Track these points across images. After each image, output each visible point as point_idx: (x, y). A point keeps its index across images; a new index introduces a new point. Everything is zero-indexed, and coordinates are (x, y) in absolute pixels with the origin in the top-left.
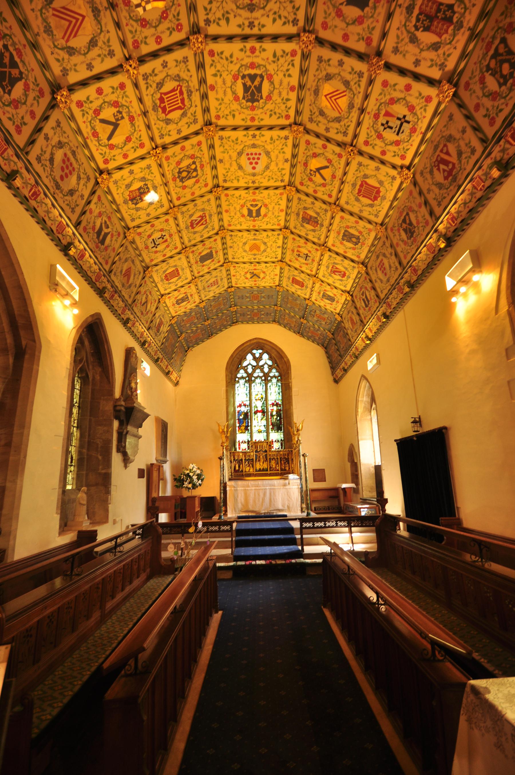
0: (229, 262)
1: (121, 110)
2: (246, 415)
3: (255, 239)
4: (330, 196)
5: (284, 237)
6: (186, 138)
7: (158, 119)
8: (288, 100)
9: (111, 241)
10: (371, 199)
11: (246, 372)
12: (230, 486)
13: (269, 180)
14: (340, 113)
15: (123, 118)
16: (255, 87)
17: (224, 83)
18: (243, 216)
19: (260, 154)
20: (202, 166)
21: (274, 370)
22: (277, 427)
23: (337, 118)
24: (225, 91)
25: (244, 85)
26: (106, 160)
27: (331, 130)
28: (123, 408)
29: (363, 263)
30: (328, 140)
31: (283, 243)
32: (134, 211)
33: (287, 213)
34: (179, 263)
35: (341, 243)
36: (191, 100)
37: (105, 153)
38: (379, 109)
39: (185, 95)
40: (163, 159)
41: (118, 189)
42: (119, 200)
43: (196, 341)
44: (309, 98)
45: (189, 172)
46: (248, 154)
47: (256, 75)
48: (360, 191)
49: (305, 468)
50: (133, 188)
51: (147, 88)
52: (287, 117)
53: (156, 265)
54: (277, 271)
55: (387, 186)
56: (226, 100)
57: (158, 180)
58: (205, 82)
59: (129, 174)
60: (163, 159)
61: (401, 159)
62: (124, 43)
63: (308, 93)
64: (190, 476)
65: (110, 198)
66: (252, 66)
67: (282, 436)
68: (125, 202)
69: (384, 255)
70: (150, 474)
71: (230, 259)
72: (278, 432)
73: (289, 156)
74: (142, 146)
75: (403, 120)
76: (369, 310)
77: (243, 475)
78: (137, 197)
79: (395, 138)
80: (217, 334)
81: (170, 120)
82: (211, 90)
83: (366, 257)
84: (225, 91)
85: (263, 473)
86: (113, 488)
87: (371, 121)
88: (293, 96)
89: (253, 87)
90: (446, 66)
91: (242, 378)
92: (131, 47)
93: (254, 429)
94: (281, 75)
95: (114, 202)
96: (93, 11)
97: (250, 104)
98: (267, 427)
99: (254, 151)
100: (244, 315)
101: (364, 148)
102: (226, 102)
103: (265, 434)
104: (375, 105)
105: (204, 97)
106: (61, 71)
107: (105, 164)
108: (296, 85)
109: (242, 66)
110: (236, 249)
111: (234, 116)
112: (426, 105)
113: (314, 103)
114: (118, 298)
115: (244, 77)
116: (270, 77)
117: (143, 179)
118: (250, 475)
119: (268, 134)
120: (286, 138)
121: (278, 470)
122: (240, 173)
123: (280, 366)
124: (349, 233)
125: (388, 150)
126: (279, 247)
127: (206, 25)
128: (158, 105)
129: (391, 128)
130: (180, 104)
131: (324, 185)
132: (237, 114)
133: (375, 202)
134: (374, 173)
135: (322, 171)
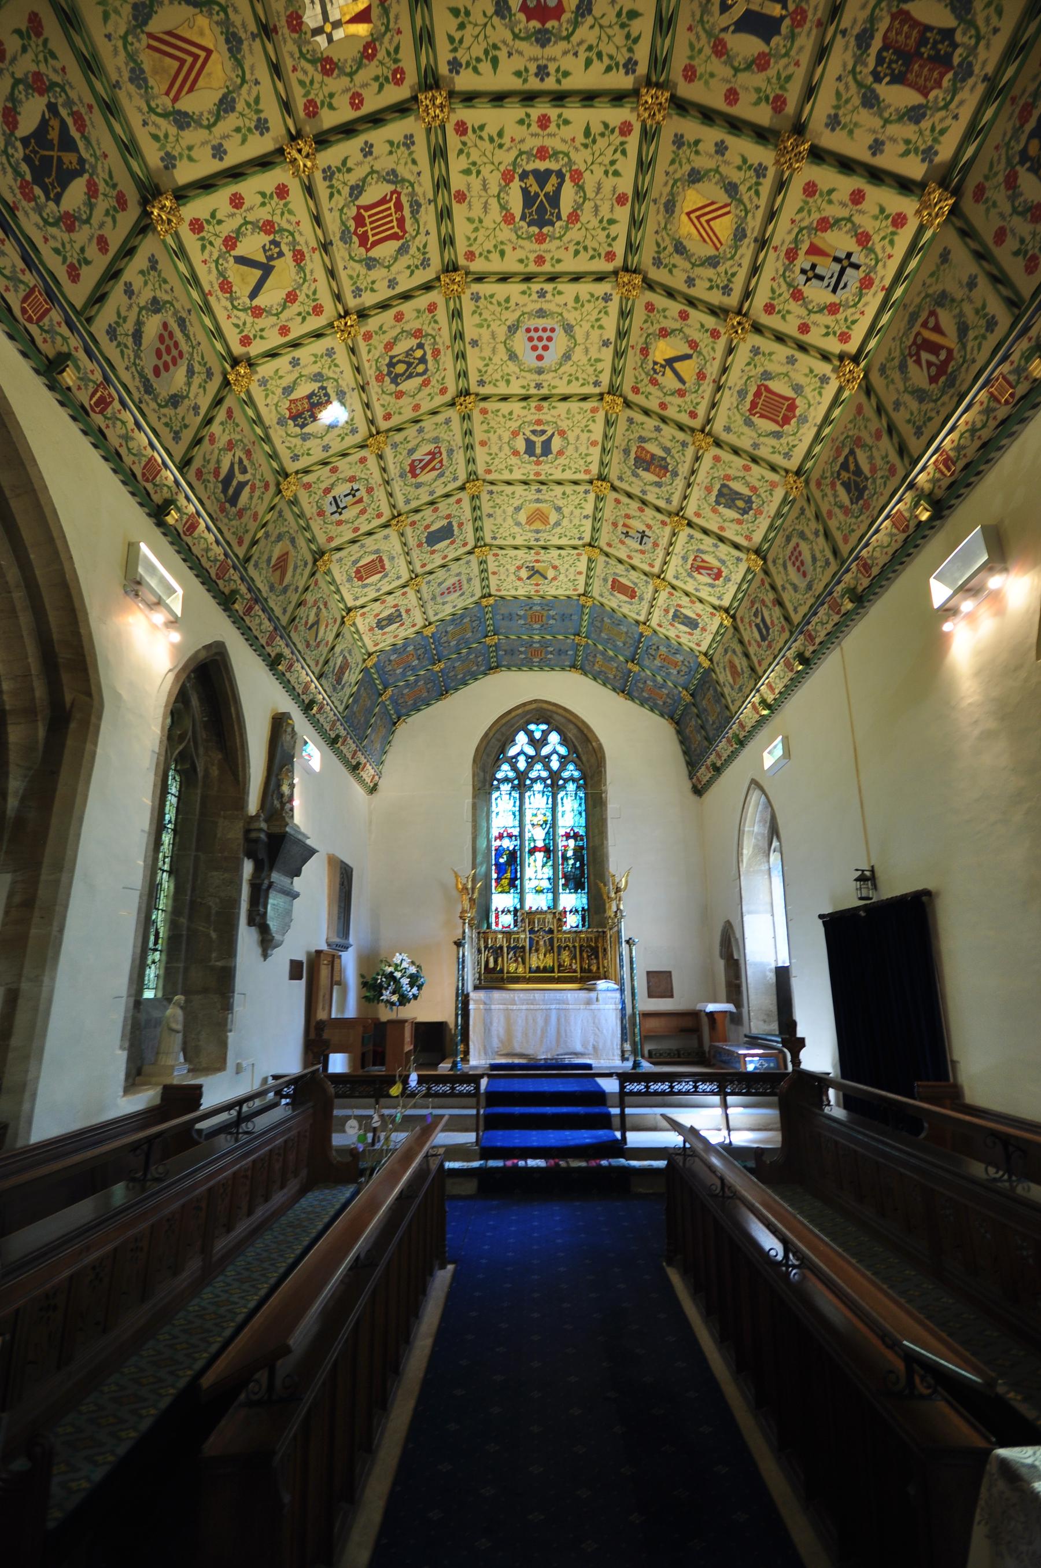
0: (485, 545)
1: (278, 239)
2: (512, 855)
3: (538, 501)
4: (693, 415)
5: (597, 497)
6: (406, 296)
7: (351, 258)
8: (611, 222)
9: (251, 498)
10: (776, 422)
11: (514, 768)
12: (476, 1002)
13: (569, 382)
14: (717, 249)
15: (281, 254)
16: (546, 195)
17: (485, 187)
18: (516, 453)
19: (553, 330)
20: (436, 353)
21: (571, 767)
22: (575, 882)
23: (710, 258)
24: (486, 203)
25: (525, 191)
26: (247, 337)
27: (697, 282)
28: (263, 836)
29: (757, 552)
30: (692, 302)
31: (596, 508)
32: (298, 441)
33: (604, 449)
34: (383, 546)
35: (714, 511)
36: (438, 362)
37: (244, 324)
38: (796, 240)
39: (407, 212)
40: (360, 338)
41: (267, 396)
42: (269, 417)
43: (415, 704)
44: (654, 218)
45: (409, 364)
46: (528, 330)
47: (548, 173)
48: (754, 404)
49: (632, 969)
50: (297, 394)
51: (331, 196)
52: (610, 256)
53: (339, 549)
54: (582, 566)
55: (810, 396)
56: (488, 222)
57: (348, 378)
58: (447, 185)
59: (290, 367)
60: (360, 338)
61: (841, 341)
62: (287, 106)
63: (653, 208)
64: (394, 979)
65: (250, 412)
66: (542, 153)
67: (585, 901)
68: (281, 422)
69: (802, 535)
70: (314, 972)
71: (488, 540)
72: (576, 892)
73: (611, 334)
74: (318, 310)
75: (846, 262)
76: (769, 646)
77: (502, 980)
78: (305, 412)
79: (829, 298)
80: (457, 689)
81: (375, 259)
82: (459, 202)
83: (765, 538)
84: (486, 203)
85: (544, 976)
86: (237, 998)
87: (779, 264)
88: (623, 214)
89: (542, 196)
90: (936, 153)
91: (506, 780)
92: (302, 114)
93: (529, 885)
94: (599, 171)
95: (259, 420)
96: (227, 41)
97: (535, 230)
98: (553, 880)
99: (541, 323)
100: (511, 652)
101: (765, 320)
102: (487, 225)
103: (550, 896)
104: (790, 232)
105: (445, 214)
106: (162, 159)
107: (244, 345)
108: (630, 193)
109: (521, 153)
110: (499, 521)
111: (502, 253)
112: (893, 233)
113: (665, 228)
114: (260, 613)
115: (524, 176)
116: (577, 177)
117: (318, 377)
118: (517, 980)
119: (570, 290)
120: (607, 298)
121: (575, 971)
122: (512, 367)
123: (584, 758)
124: (731, 489)
125: (814, 323)
126: (586, 517)
127: (451, 71)
128: (352, 229)
129: (821, 278)
130: (396, 230)
131: (681, 393)
132: (508, 249)
133: (786, 427)
134: (783, 369)
135: (676, 365)
